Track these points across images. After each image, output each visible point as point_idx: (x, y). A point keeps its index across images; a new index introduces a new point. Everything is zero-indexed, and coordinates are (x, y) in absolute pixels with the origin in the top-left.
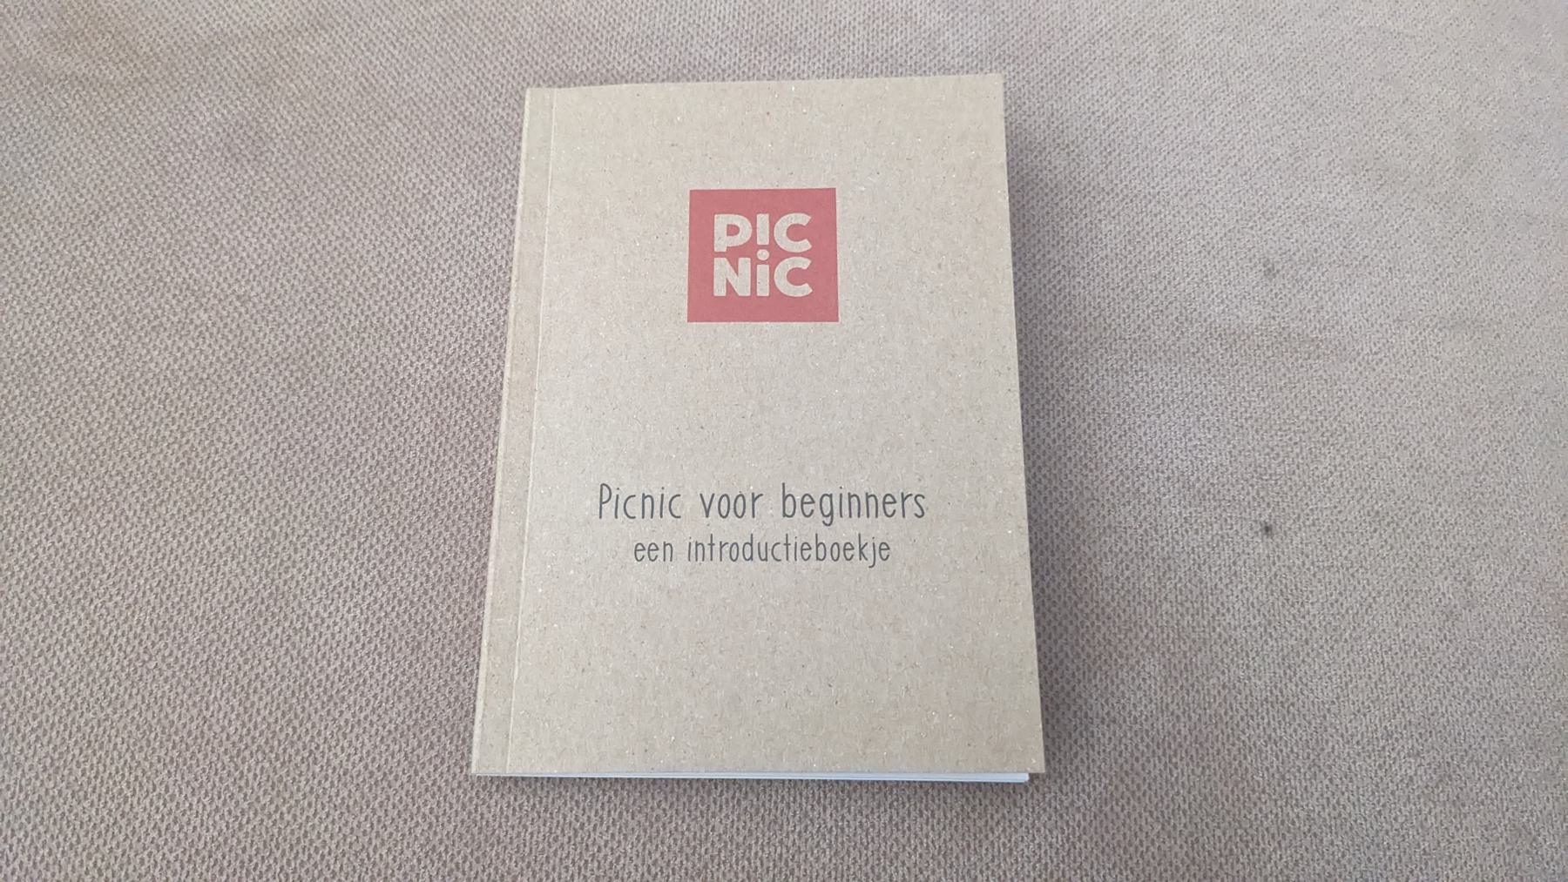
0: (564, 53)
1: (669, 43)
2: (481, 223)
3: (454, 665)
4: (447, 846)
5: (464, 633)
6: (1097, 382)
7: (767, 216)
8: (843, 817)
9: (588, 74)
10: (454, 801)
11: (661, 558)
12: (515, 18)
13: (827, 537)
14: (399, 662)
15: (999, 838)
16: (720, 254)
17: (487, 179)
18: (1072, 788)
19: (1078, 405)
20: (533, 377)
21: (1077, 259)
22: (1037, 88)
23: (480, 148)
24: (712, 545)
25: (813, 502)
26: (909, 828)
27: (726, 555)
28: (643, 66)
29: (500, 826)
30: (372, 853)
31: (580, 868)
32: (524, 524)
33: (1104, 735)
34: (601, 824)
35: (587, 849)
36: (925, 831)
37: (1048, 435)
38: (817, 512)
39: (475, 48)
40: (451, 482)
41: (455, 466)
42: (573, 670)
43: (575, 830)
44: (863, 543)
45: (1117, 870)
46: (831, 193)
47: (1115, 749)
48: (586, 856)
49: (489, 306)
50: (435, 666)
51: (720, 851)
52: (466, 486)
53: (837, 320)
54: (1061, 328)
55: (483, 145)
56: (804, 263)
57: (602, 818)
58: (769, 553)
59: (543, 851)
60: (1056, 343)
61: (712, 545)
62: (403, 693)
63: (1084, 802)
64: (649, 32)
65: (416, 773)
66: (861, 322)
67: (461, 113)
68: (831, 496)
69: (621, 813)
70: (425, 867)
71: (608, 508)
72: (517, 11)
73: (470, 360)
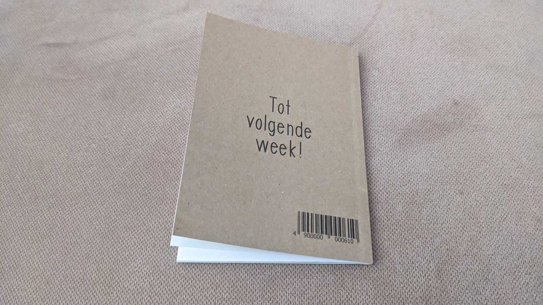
11: (286, 132)
40: (168, 191)
41: (170, 186)
47: (405, 273)
62: (149, 261)
67: (176, 78)
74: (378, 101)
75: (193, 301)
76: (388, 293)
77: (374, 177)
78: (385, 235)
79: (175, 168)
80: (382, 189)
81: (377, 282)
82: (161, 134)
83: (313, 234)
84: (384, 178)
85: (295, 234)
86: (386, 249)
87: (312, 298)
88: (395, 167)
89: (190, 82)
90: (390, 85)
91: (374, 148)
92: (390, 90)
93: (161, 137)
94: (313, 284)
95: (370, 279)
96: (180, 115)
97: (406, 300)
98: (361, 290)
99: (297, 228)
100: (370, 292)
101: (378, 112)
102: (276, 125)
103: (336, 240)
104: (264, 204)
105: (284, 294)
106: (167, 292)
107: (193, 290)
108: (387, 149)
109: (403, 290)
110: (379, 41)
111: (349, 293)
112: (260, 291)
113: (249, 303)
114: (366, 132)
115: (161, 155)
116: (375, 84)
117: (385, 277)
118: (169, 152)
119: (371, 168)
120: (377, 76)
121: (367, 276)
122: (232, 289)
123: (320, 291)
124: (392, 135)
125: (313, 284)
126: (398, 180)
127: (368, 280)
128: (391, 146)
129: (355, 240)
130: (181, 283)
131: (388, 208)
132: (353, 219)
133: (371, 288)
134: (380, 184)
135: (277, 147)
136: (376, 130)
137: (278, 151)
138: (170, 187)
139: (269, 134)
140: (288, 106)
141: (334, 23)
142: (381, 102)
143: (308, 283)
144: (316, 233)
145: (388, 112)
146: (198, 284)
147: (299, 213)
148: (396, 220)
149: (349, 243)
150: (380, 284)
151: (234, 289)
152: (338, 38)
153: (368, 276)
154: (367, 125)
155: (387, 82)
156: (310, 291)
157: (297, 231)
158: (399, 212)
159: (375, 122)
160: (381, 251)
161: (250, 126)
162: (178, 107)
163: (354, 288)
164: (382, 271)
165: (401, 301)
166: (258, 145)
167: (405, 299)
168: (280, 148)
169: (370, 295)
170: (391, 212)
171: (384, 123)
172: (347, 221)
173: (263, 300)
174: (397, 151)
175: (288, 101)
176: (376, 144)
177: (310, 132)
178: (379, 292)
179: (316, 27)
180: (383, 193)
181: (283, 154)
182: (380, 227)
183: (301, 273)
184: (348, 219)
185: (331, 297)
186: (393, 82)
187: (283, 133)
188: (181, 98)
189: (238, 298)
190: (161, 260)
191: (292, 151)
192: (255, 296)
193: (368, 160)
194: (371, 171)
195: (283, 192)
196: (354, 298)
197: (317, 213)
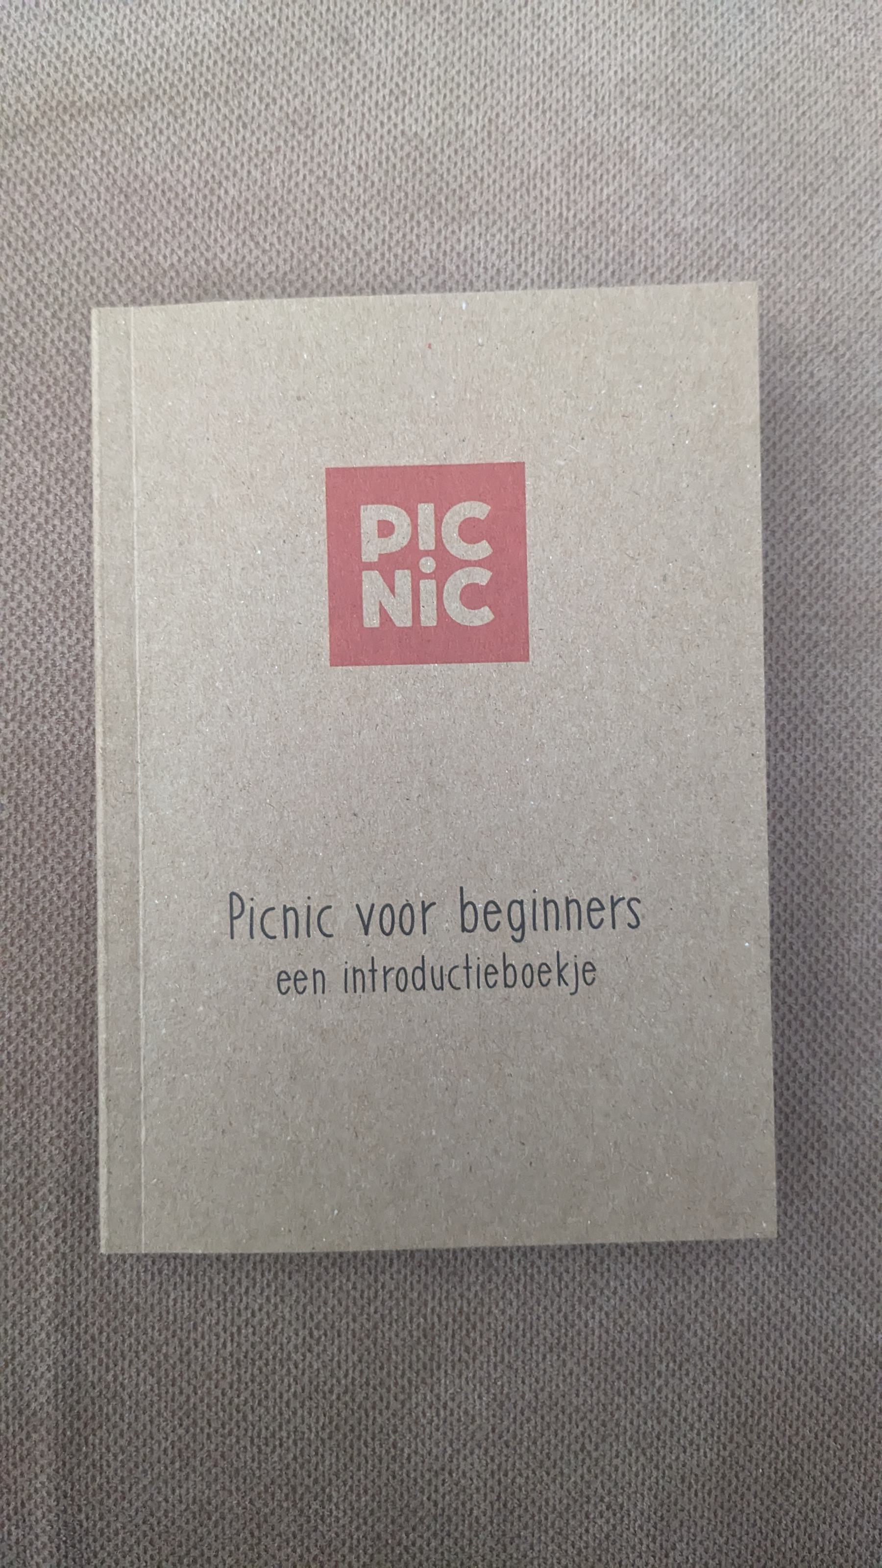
0: (146, 234)
1: (289, 211)
2: (50, 512)
3: (67, 1112)
4: (79, 1319)
5: (75, 1072)
7: (431, 506)
9: (181, 268)
11: (310, 989)
12: (72, 178)
13: (518, 956)
15: (711, 1272)
16: (370, 566)
17: (52, 444)
19: (833, 729)
20: (133, 744)
21: (842, 518)
22: (799, 258)
23: (40, 395)
24: (373, 971)
25: (499, 911)
27: (391, 984)
28: (256, 252)
29: (138, 1293)
31: (232, 1335)
32: (137, 945)
34: (254, 1287)
35: (239, 1314)
36: (626, 1271)
37: (794, 774)
38: (505, 923)
39: (19, 231)
40: (42, 883)
41: (45, 861)
42: (211, 1132)
44: (562, 965)
46: (517, 470)
48: (239, 1321)
49: (70, 635)
50: (45, 1114)
52: (61, 887)
53: (526, 658)
54: (816, 622)
55: (44, 389)
56: (482, 577)
57: (254, 1279)
58: (446, 980)
59: (189, 1319)
60: (810, 644)
61: (373, 971)
64: (263, 195)
65: (36, 1239)
66: (559, 662)
68: (521, 903)
69: (276, 1273)
70: (56, 1343)
71: (242, 925)
72: (74, 166)
73: (51, 714)
118: (22, 713)
152: (686, 177)
190: (51, 1142)
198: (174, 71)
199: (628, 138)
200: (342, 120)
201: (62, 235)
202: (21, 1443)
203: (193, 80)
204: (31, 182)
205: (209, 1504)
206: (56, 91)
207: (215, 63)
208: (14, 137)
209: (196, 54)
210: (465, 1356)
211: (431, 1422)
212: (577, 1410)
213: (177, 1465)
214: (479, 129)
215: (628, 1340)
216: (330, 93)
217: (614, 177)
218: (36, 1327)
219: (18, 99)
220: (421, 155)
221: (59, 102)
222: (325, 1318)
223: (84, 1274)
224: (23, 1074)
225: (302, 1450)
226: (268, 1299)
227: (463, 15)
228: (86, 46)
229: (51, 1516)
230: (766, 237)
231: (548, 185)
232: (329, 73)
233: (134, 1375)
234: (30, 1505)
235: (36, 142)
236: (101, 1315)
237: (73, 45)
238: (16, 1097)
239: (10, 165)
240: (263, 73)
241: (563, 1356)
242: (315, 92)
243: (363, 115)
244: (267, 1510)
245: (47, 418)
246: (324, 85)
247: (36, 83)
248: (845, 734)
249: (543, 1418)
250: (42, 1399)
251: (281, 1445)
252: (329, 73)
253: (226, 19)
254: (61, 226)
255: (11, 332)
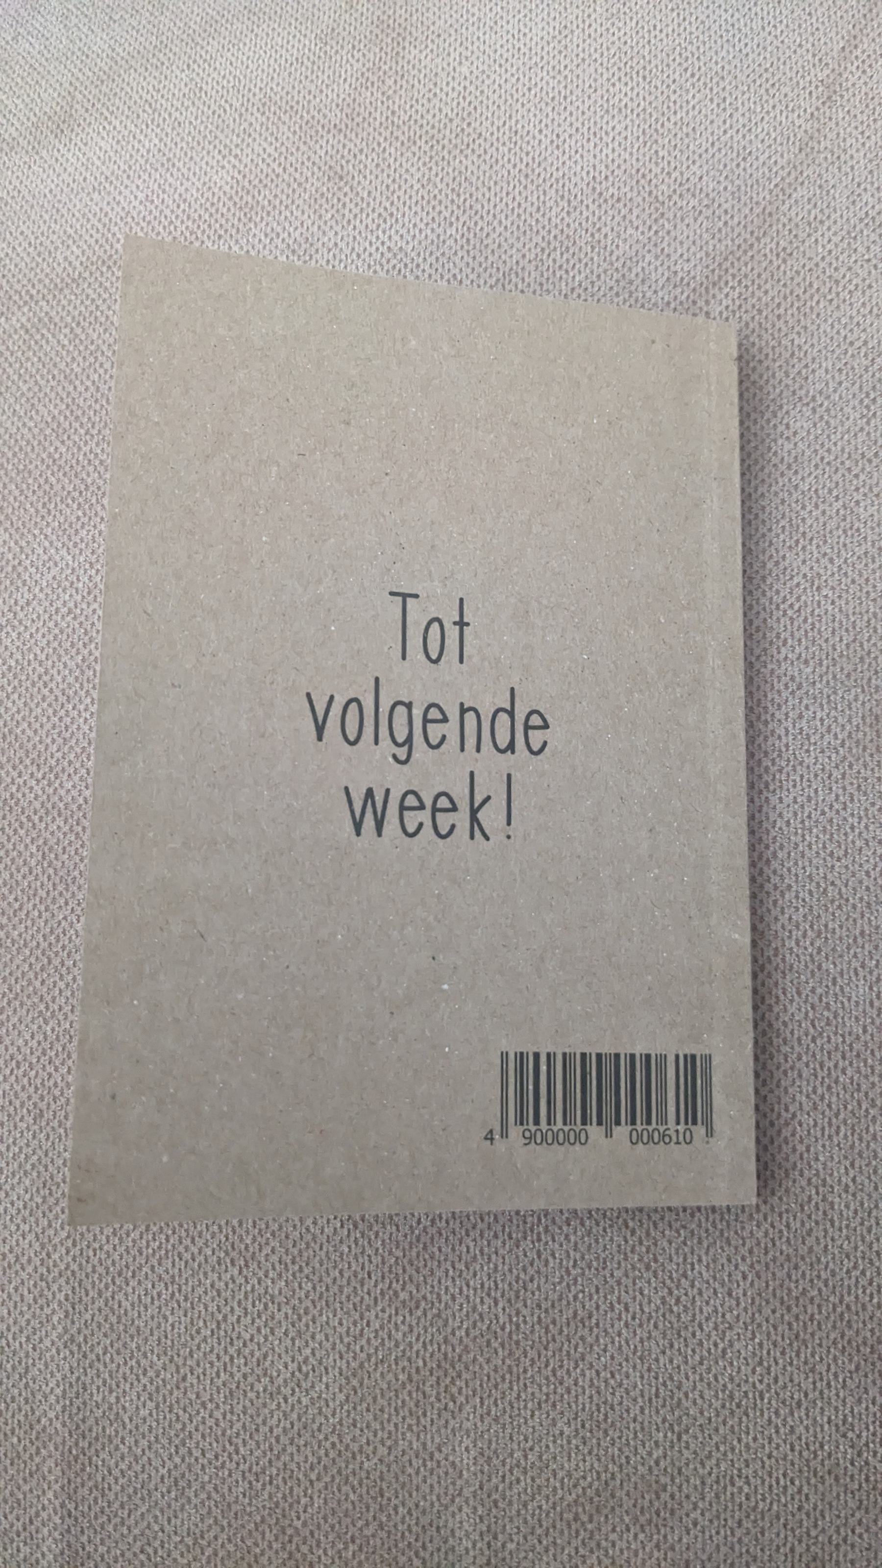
4: (85, 1336)
6: (850, 736)
8: (518, 1313)
10: (89, 1287)
11: (453, 739)
14: (22, 1132)
18: (804, 1274)
26: (597, 1325)
29: (139, 1316)
30: (11, 1341)
33: (847, 1206)
35: (232, 1344)
39: (62, 366)
40: (63, 923)
41: (67, 903)
43: (218, 1323)
45: (861, 1373)
47: (862, 1224)
48: (232, 1351)
51: (377, 1349)
62: (28, 1167)
63: (820, 1290)
65: (48, 1255)
67: (50, 456)
70: (65, 1359)
74: (804, 548)
75: (178, 1302)
76: (800, 1288)
77: (775, 872)
78: (801, 1092)
79: (77, 834)
80: (801, 919)
81: (766, 1253)
82: (16, 696)
83: (555, 1129)
84: (810, 876)
85: (492, 1139)
86: (801, 1142)
87: (550, 1303)
88: (852, 828)
89: (100, 477)
90: (857, 476)
91: (780, 756)
92: (857, 497)
93: (18, 712)
94: (555, 1258)
95: (744, 1245)
96: (75, 618)
97: (857, 1313)
98: (711, 1281)
99: (499, 1114)
100: (738, 1286)
101: (803, 598)
102: (417, 713)
103: (634, 1140)
104: (381, 1042)
105: (461, 1289)
106: (94, 1267)
107: (174, 1265)
108: (830, 758)
109: (850, 1278)
110: (822, 265)
111: (670, 1289)
112: (383, 1277)
113: (350, 1316)
114: (754, 690)
115: (25, 782)
116: (796, 472)
117: (792, 1236)
119: (765, 837)
120: (808, 432)
121: (732, 1233)
122: (297, 1268)
123: (575, 1283)
124: (852, 697)
125: (555, 1258)
126: (861, 882)
127: (736, 1248)
128: (843, 745)
129: (700, 1131)
130: (134, 1241)
131: (819, 991)
132: (694, 1052)
133: (743, 1273)
134: (797, 897)
135: (422, 807)
136: (792, 678)
137: (428, 823)
138: (69, 908)
139: (391, 759)
140: (461, 624)
141: (642, 182)
142: (815, 552)
143: (539, 1257)
144: (565, 1124)
145: (840, 597)
146: (187, 1249)
147: (504, 1056)
148: (843, 1036)
149: (678, 1143)
150: (774, 1260)
151: (301, 1270)
152: (657, 257)
153: (736, 1233)
154: (758, 657)
155: (842, 463)
156: (543, 1280)
157: (497, 1129)
158: (857, 1003)
159: (790, 641)
160: (784, 1147)
161: (320, 739)
162: (68, 584)
163: (689, 1273)
164: (785, 1216)
165: (842, 1314)
166: (352, 812)
167: (853, 1308)
168: (435, 810)
169: (741, 1295)
170: (828, 1004)
171: (824, 645)
172: (673, 1064)
173: (393, 1307)
174: (865, 766)
175: (461, 600)
176: (791, 737)
177: (546, 726)
178: (771, 1288)
179: (574, 203)
180: (805, 935)
181: (443, 832)
182: (786, 1061)
183: (515, 1221)
184: (677, 1057)
185: (611, 1303)
186: (870, 461)
187: (444, 746)
188: (75, 545)
189: (316, 1298)
191: (480, 815)
192: (369, 1293)
193: (757, 804)
194: (767, 847)
195: (446, 987)
196: (685, 1306)
197: (567, 1051)
198: (194, 221)
199: (599, 229)
200: (336, 244)
201: (97, 365)
202: (31, 1458)
203: (210, 226)
204: (74, 325)
205: (202, 1537)
206: (97, 248)
207: (229, 209)
208: (61, 290)
209: (213, 204)
210: (451, 1404)
211: (417, 1473)
212: (569, 1475)
213: (173, 1495)
214: (458, 237)
215: (621, 1403)
216: (326, 222)
217: (586, 264)
218: (47, 1343)
219: (66, 258)
220: (406, 265)
221: (99, 257)
222: (313, 1354)
223: (91, 1294)
224: (42, 1098)
225: (291, 1489)
226: (259, 1330)
227: (446, 142)
228: (123, 208)
229: (56, 1535)
230: (737, 303)
231: (523, 280)
232: (325, 206)
233: (135, 1398)
234: (37, 1523)
235: (78, 292)
236: (105, 1335)
237: (112, 209)
238: (35, 1119)
239: (58, 313)
240: (268, 213)
241: (552, 1415)
242: (313, 223)
243: (355, 238)
244: (258, 1550)
245: (78, 518)
246: (320, 217)
247: (81, 243)
248: (836, 774)
249: (533, 1480)
250: (51, 1415)
251: (271, 1483)
252: (325, 206)
253: (239, 172)
254: (96, 358)
255: (52, 449)
